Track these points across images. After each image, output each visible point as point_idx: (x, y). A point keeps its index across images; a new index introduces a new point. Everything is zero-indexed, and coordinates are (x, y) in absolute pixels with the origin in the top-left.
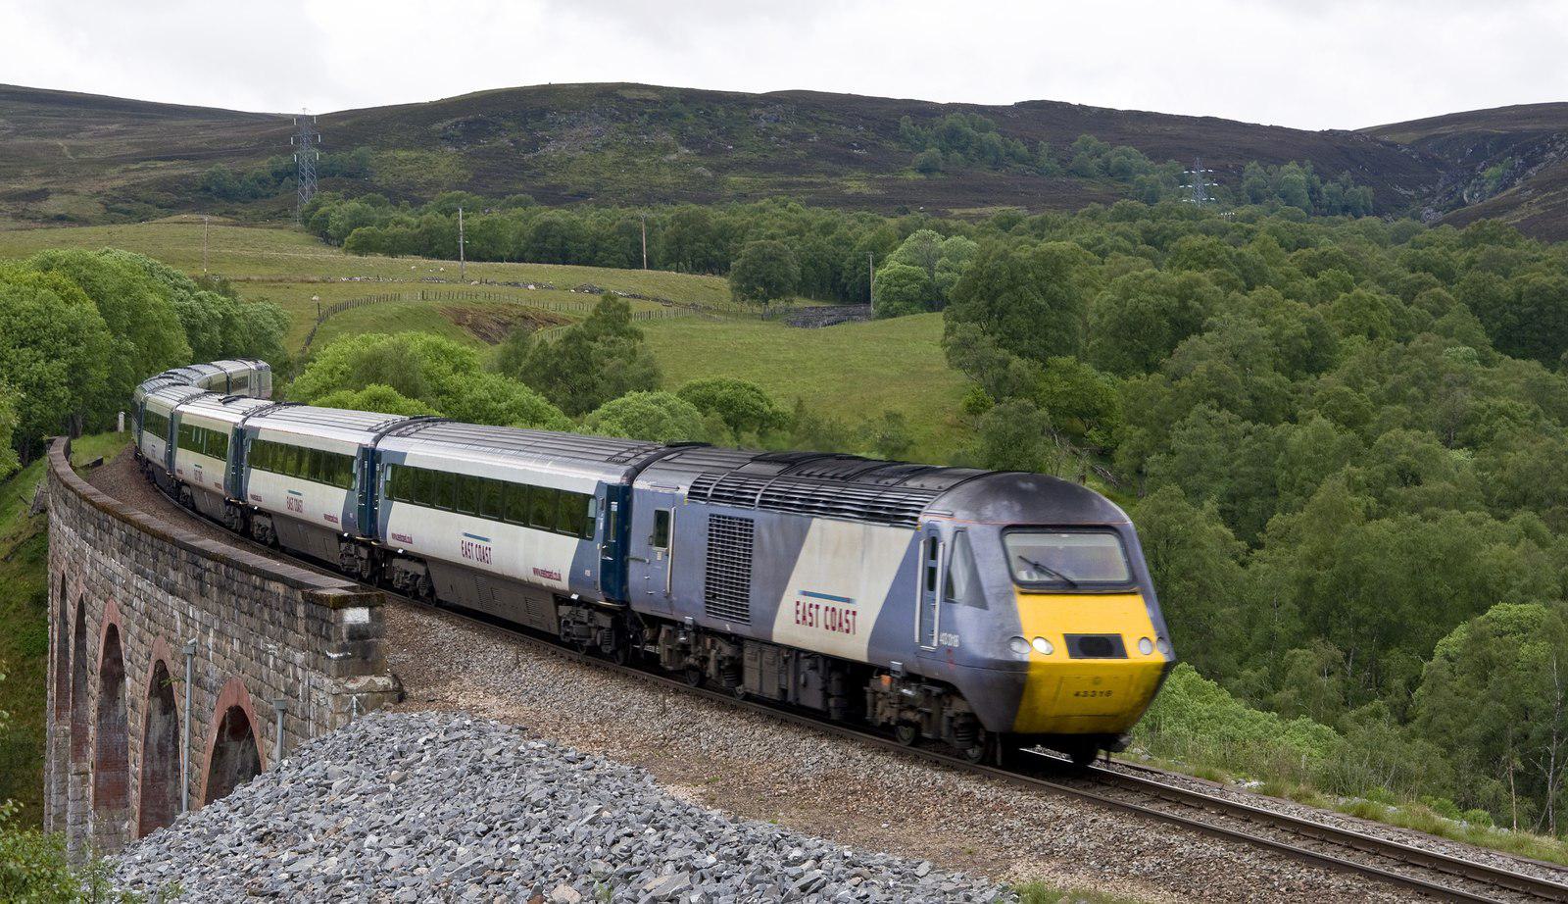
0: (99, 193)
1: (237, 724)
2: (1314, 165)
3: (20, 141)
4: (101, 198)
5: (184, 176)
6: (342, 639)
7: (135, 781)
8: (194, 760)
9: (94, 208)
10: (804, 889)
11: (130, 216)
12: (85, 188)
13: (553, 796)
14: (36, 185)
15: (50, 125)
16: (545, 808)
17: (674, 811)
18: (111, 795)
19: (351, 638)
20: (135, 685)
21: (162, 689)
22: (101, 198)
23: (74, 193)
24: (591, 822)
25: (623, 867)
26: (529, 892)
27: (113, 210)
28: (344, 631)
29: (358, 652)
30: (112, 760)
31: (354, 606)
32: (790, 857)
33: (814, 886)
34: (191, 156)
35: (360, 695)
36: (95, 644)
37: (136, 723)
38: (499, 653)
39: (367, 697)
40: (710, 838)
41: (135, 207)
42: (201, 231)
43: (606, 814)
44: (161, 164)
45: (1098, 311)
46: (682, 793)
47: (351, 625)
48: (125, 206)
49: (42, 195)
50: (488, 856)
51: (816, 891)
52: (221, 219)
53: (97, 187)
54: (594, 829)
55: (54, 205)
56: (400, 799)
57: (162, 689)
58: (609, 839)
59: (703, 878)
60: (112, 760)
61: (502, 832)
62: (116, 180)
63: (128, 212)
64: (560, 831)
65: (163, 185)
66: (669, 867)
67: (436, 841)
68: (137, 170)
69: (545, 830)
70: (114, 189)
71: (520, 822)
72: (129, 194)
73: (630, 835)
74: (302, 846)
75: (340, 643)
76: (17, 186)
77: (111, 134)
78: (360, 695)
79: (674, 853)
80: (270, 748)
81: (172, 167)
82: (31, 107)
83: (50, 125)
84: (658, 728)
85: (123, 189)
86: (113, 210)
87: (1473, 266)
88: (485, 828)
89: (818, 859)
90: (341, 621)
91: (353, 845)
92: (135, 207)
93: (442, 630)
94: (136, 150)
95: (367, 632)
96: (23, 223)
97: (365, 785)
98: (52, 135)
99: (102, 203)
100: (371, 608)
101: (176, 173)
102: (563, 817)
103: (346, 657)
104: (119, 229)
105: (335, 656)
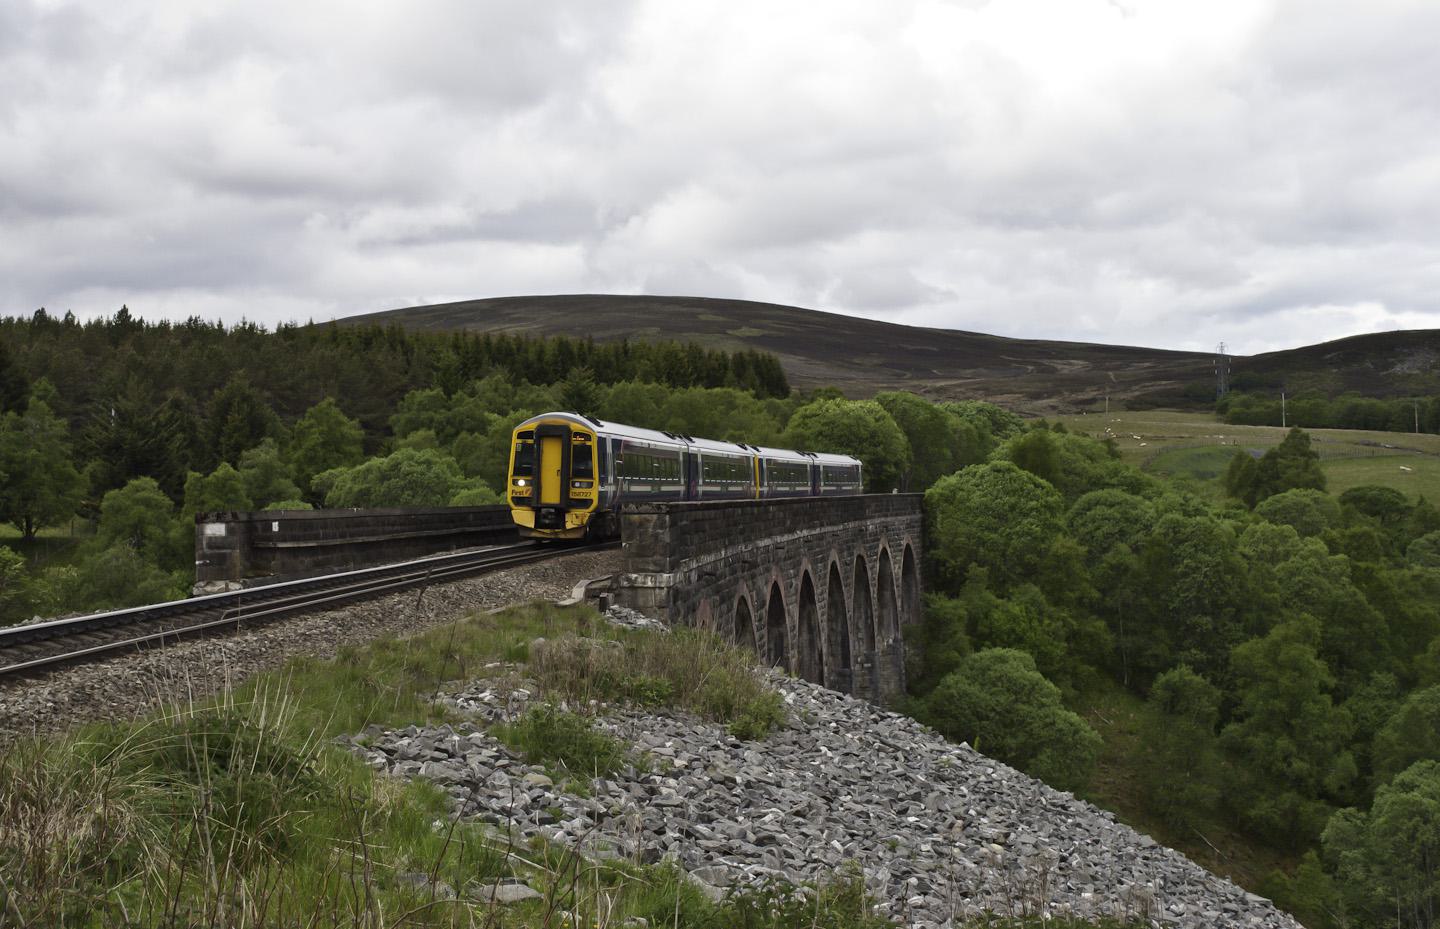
19: (210, 546)
28: (204, 543)
47: (210, 538)
81: (1171, 384)
90: (202, 534)
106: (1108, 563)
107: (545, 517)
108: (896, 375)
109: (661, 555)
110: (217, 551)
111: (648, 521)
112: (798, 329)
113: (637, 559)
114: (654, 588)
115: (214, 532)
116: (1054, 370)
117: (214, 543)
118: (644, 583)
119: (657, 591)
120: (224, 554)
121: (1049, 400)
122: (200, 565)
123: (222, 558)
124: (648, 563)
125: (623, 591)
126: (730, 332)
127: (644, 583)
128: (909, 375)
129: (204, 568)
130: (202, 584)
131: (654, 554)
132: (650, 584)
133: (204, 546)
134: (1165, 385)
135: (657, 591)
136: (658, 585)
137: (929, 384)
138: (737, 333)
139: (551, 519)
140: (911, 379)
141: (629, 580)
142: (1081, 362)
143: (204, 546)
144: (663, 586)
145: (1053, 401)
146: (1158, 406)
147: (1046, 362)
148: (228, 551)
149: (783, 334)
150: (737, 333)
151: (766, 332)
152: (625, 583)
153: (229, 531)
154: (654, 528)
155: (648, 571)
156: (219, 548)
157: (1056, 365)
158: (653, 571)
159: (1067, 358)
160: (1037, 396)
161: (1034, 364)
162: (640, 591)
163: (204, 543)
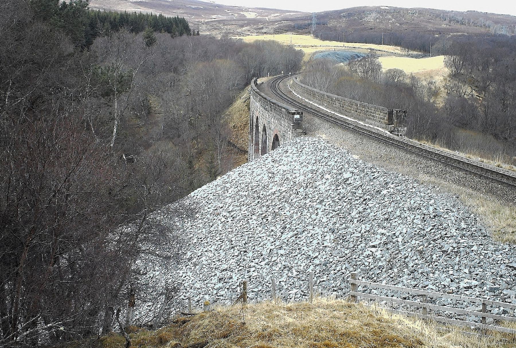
1: (276, 138)
2: (490, 90)
3: (259, 17)
7: (260, 148)
8: (269, 143)
10: (374, 178)
12: (270, 27)
13: (329, 156)
16: (327, 158)
17: (352, 160)
18: (257, 151)
20: (261, 129)
21: (264, 130)
24: (335, 162)
25: (340, 172)
26: (321, 176)
30: (257, 144)
32: (373, 171)
33: (376, 178)
36: (255, 120)
37: (261, 137)
38: (327, 125)
40: (358, 167)
43: (339, 160)
46: (356, 157)
49: (262, 28)
50: (314, 168)
51: (376, 179)
54: (336, 163)
55: (264, 31)
56: (300, 155)
57: (264, 130)
58: (338, 165)
59: (355, 175)
60: (257, 144)
61: (318, 163)
62: (276, 26)
64: (329, 164)
65: (286, 26)
66: (349, 172)
67: (306, 164)
69: (326, 163)
71: (322, 161)
72: (279, 28)
73: (342, 165)
74: (280, 164)
79: (350, 169)
80: (281, 142)
84: (354, 143)
88: (315, 162)
89: (379, 172)
91: (290, 164)
93: (317, 121)
94: (281, 19)
97: (294, 152)
98: (265, 16)
102: (87, 224)
105: (292, 125)
145: (248, 28)
147: (241, 13)
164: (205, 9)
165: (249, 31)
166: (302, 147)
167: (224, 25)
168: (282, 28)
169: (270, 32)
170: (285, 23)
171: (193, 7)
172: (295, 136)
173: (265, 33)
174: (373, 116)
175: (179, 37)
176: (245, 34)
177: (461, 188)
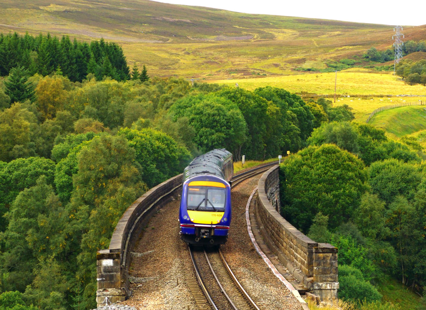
0: (325, 59)
4: (325, 62)
5: (359, 52)
6: (101, 272)
9: (323, 66)
11: (336, 69)
14: (301, 56)
15: (313, 32)
19: (105, 271)
22: (325, 62)
23: (315, 60)
27: (330, 66)
28: (102, 269)
29: (108, 278)
31: (106, 258)
34: (363, 44)
35: (108, 296)
39: (112, 298)
41: (339, 65)
42: (351, 75)
44: (351, 47)
45: (180, 66)
47: (105, 267)
48: (335, 65)
49: (303, 60)
52: (367, 70)
53: (325, 57)
55: (307, 65)
62: (332, 54)
63: (336, 67)
65: (349, 56)
68: (341, 50)
70: (331, 58)
72: (337, 59)
75: (100, 274)
76: (295, 57)
77: (335, 36)
78: (108, 296)
81: (355, 49)
82: (306, 25)
83: (313, 32)
85: (334, 58)
86: (330, 66)
87: (309, 294)
90: (101, 265)
92: (339, 65)
95: (112, 269)
96: (296, 72)
99: (326, 64)
100: (114, 259)
101: (356, 51)
103: (102, 280)
104: (321, 74)
106: (393, 210)
107: (203, 234)
108: (162, 40)
109: (335, 273)
110: (108, 274)
111: (327, 256)
112: (91, 6)
113: (322, 275)
114: (330, 290)
115: (107, 264)
116: (272, 37)
117: (107, 269)
118: (326, 287)
119: (332, 291)
120: (113, 275)
121: (273, 60)
122: (100, 281)
123: (111, 277)
124: (328, 277)
125: (315, 291)
126: (41, 8)
127: (326, 287)
128: (171, 40)
129: (102, 282)
130: (101, 290)
131: (331, 273)
132: (329, 288)
133: (102, 271)
134: (351, 49)
135: (332, 291)
136: (333, 288)
137: (186, 46)
138: (47, 9)
139: (206, 235)
140: (172, 43)
141: (318, 286)
142: (290, 31)
143: (102, 271)
144: (335, 288)
145: (276, 60)
146: (353, 65)
147: (266, 30)
148: (115, 273)
149: (80, 10)
150: (47, 9)
151: (68, 8)
152: (316, 288)
153: (115, 263)
154: (331, 260)
155: (328, 281)
156: (109, 272)
157: (273, 33)
158: (330, 281)
159: (280, 27)
160: (264, 57)
161: (259, 32)
162: (323, 291)
163: (102, 269)
164: (194, 24)
165: (276, 65)
166: (306, 253)
167: (230, 55)
168: (342, 60)
169: (319, 68)
170: (350, 50)
171: (171, 20)
172: (105, 303)
173: (309, 70)
174: (403, 300)
175: (336, 301)
176: (268, 73)
177: (103, 243)
